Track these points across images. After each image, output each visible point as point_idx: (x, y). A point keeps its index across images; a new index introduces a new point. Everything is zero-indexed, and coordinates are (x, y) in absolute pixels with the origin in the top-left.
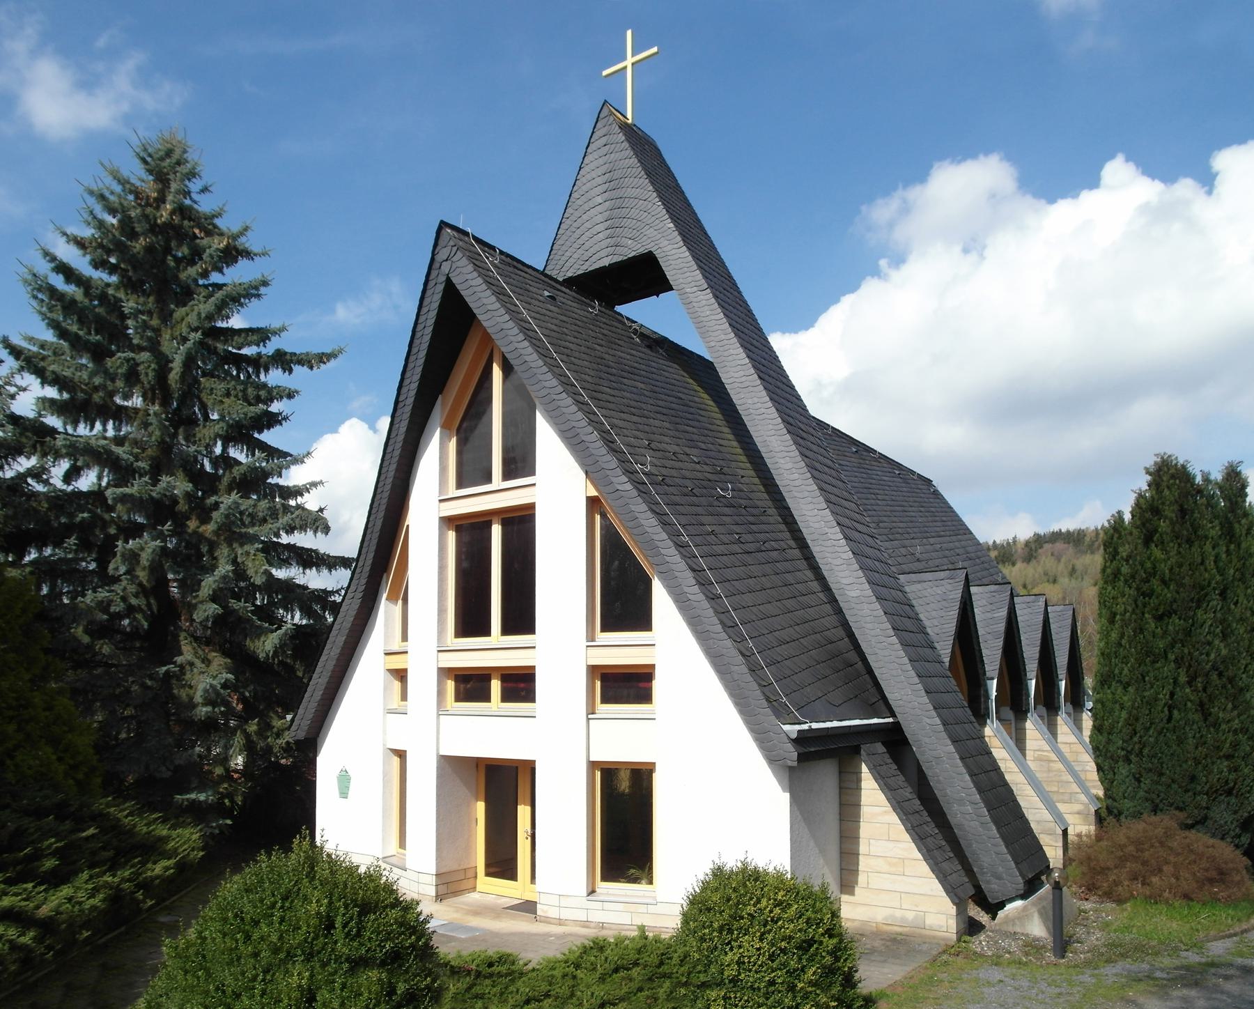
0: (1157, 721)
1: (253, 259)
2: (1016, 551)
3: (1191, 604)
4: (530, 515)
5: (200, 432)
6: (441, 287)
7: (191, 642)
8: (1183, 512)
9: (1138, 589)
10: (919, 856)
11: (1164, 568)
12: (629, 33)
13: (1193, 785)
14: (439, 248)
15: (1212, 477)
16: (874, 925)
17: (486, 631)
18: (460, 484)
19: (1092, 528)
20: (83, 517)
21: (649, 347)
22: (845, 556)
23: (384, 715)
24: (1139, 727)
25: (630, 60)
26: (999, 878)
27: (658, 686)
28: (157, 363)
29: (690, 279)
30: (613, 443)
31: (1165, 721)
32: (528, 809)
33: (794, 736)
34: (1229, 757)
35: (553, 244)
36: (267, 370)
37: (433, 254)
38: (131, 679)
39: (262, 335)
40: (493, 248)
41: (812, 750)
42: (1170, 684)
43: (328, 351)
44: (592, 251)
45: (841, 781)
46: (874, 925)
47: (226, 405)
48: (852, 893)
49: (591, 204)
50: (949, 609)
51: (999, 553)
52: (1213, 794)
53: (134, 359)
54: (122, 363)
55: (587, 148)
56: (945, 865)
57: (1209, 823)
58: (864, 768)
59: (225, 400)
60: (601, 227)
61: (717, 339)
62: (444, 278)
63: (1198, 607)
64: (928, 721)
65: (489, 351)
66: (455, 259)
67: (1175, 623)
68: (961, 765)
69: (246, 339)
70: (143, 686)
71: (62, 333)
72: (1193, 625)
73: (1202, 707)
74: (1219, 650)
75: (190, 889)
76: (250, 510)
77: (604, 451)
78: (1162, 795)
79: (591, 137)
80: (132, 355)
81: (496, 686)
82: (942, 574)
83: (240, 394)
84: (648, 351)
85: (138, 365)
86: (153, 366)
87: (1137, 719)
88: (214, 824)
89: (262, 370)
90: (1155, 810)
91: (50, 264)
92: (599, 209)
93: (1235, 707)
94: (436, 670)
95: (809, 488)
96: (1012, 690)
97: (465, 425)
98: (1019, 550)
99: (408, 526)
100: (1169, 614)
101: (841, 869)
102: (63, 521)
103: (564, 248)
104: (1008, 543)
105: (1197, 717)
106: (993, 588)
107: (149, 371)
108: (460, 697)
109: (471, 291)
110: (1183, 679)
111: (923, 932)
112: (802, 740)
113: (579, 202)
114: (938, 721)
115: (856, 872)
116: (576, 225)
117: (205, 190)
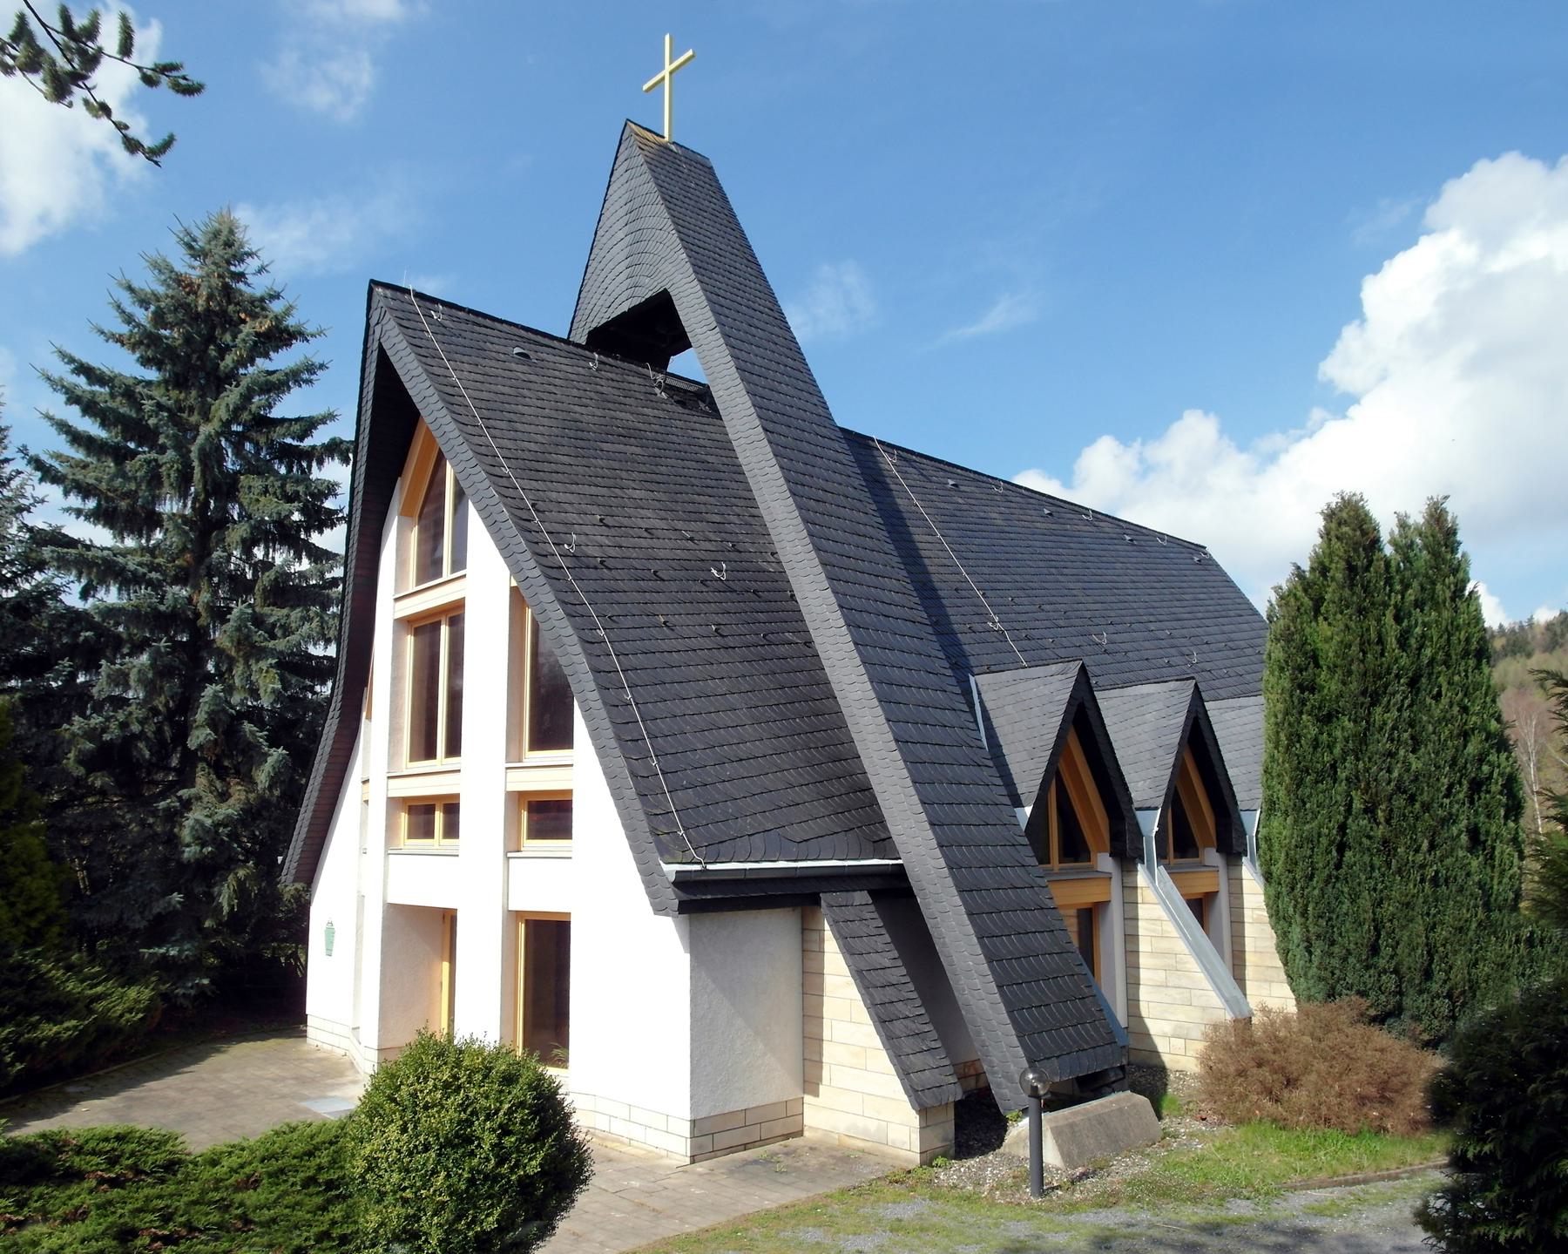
0: (1321, 865)
1: (308, 341)
2: (1533, 638)
3: (1362, 699)
4: (459, 616)
6: (375, 354)
7: (209, 774)
12: (667, 38)
13: (1376, 959)
15: (1411, 521)
16: (837, 1136)
21: (682, 403)
25: (666, 73)
30: (529, 521)
31: (1332, 865)
32: (446, 965)
35: (580, 292)
36: (320, 463)
39: (309, 425)
41: (709, 897)
42: (1339, 813)
44: (615, 295)
45: (803, 941)
46: (837, 1136)
47: (261, 504)
48: (816, 1094)
50: (1052, 715)
51: (1508, 641)
54: (142, 466)
55: (611, 177)
56: (918, 1061)
59: (262, 499)
61: (725, 387)
63: (1373, 704)
64: (933, 862)
68: (968, 922)
69: (288, 428)
71: (76, 438)
72: (1367, 729)
75: (143, 1059)
76: (283, 621)
78: (1337, 972)
79: (615, 163)
82: (1054, 668)
83: (278, 491)
84: (680, 409)
85: (160, 466)
88: (190, 985)
89: (314, 464)
91: (68, 366)
94: (385, 800)
96: (1218, 825)
97: (426, 510)
98: (1539, 636)
101: (804, 1059)
102: (64, 641)
103: (590, 295)
104: (1522, 627)
106: (1172, 685)
107: (172, 472)
111: (885, 1148)
112: (682, 882)
114: (942, 862)
115: (819, 1063)
116: (601, 266)
117: (261, 270)
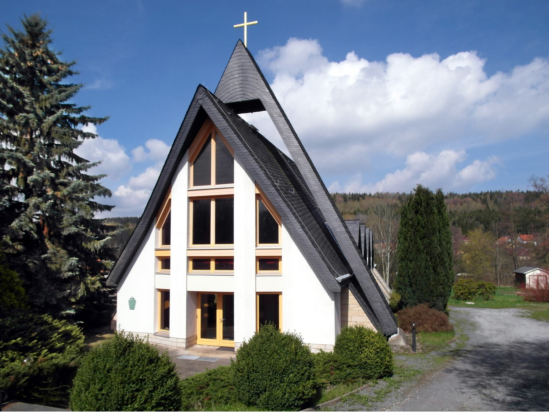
5: (54, 150)
6: (197, 109)
8: (428, 204)
9: (415, 229)
10: (369, 321)
11: (423, 222)
13: (431, 294)
14: (197, 94)
17: (208, 242)
18: (195, 184)
19: (333, 193)
20: (7, 187)
22: (335, 217)
23: (155, 275)
24: (415, 275)
26: (389, 327)
27: (281, 264)
28: (37, 119)
29: (275, 112)
33: (340, 281)
34: (442, 284)
37: (195, 96)
38: (29, 260)
40: (217, 98)
43: (103, 117)
44: (233, 95)
49: (233, 77)
52: (437, 296)
53: (27, 117)
54: (23, 118)
57: (436, 306)
58: (350, 291)
60: (237, 86)
62: (199, 106)
64: (365, 275)
65: (210, 133)
66: (204, 99)
67: (426, 241)
70: (34, 263)
73: (434, 268)
74: (438, 250)
77: (266, 178)
80: (26, 115)
81: (213, 264)
86: (36, 120)
87: (415, 272)
90: (420, 302)
92: (237, 79)
93: (443, 268)
95: (322, 192)
99: (170, 200)
100: (424, 237)
105: (432, 271)
108: (194, 268)
109: (211, 112)
110: (429, 259)
113: (228, 75)
